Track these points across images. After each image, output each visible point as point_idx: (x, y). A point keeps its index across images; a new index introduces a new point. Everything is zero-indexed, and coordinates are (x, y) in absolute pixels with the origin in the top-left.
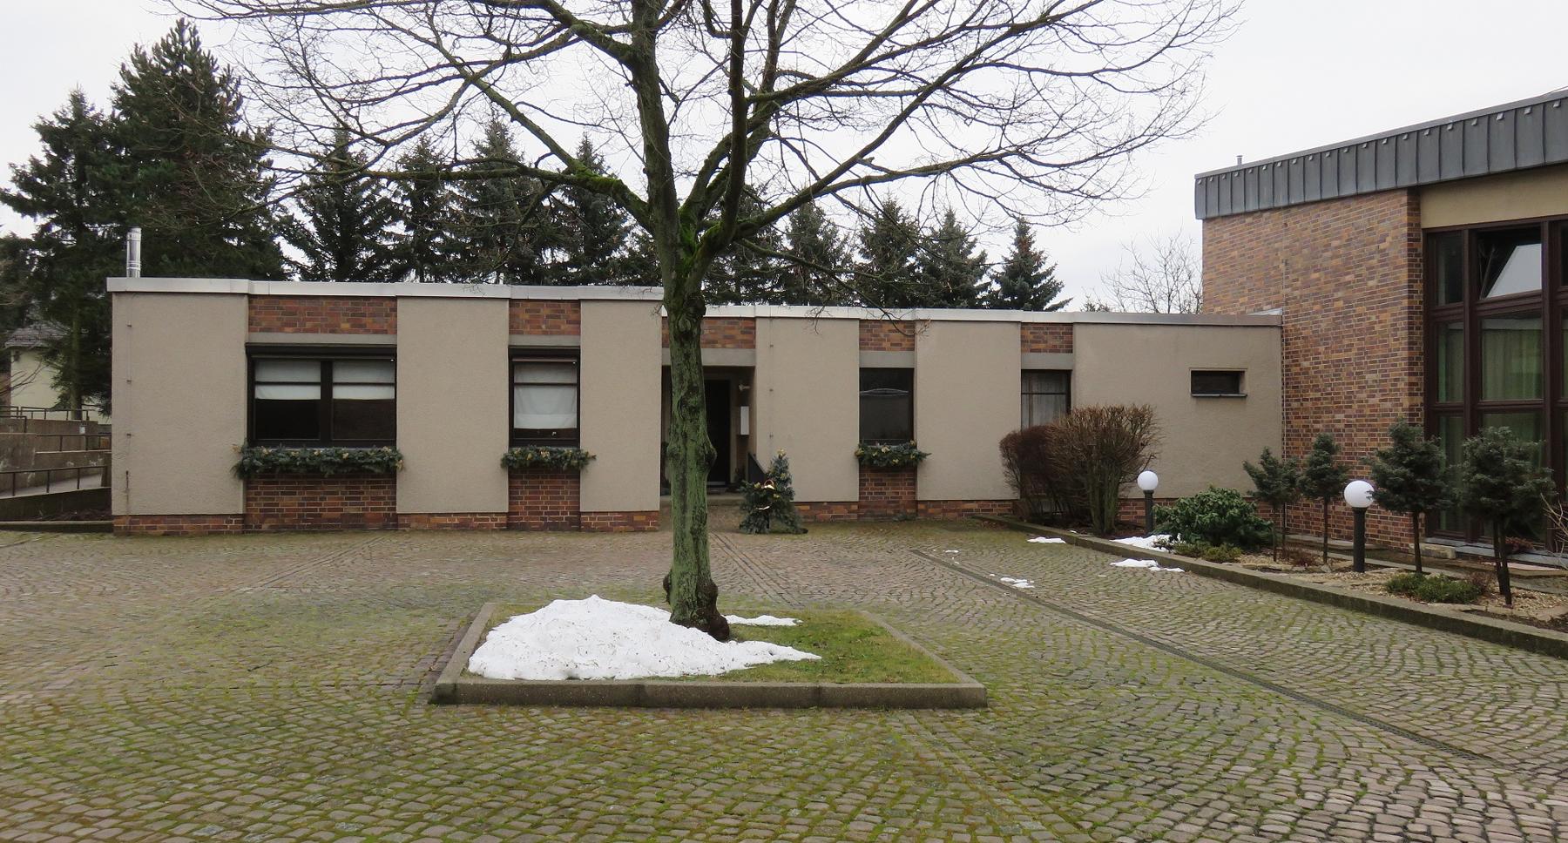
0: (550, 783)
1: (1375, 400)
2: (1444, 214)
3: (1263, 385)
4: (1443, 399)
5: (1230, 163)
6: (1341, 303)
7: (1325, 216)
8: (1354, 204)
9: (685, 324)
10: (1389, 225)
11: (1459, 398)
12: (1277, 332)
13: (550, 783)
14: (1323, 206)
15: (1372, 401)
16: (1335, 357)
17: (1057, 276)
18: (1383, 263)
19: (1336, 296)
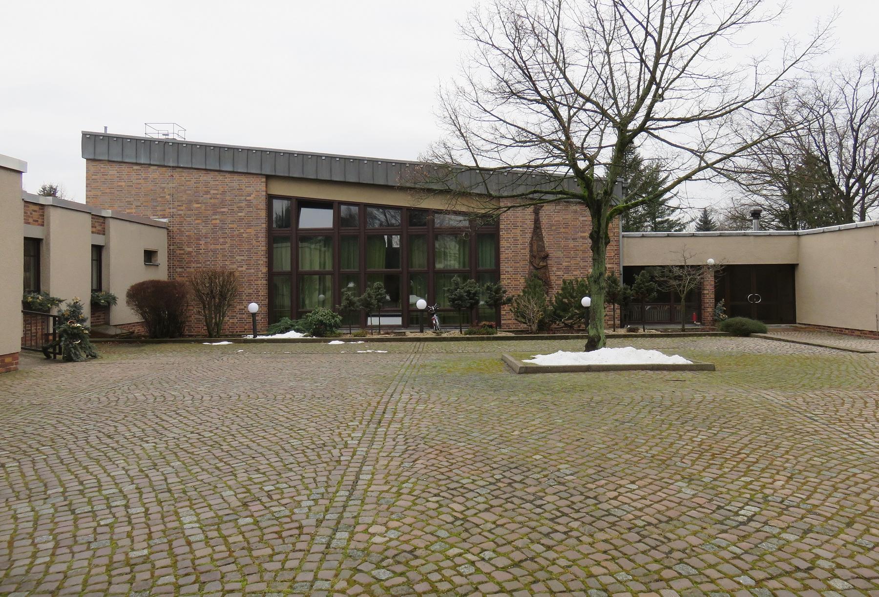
0: (402, 472)
1: (244, 269)
2: (279, 189)
3: (162, 258)
4: (300, 269)
5: (100, 130)
6: (218, 221)
7: (205, 177)
8: (228, 175)
9: (596, 257)
10: (256, 189)
11: (287, 267)
12: (165, 231)
13: (402, 472)
14: (203, 172)
15: (240, 269)
16: (212, 247)
17: (48, 186)
18: (249, 206)
19: (214, 217)
